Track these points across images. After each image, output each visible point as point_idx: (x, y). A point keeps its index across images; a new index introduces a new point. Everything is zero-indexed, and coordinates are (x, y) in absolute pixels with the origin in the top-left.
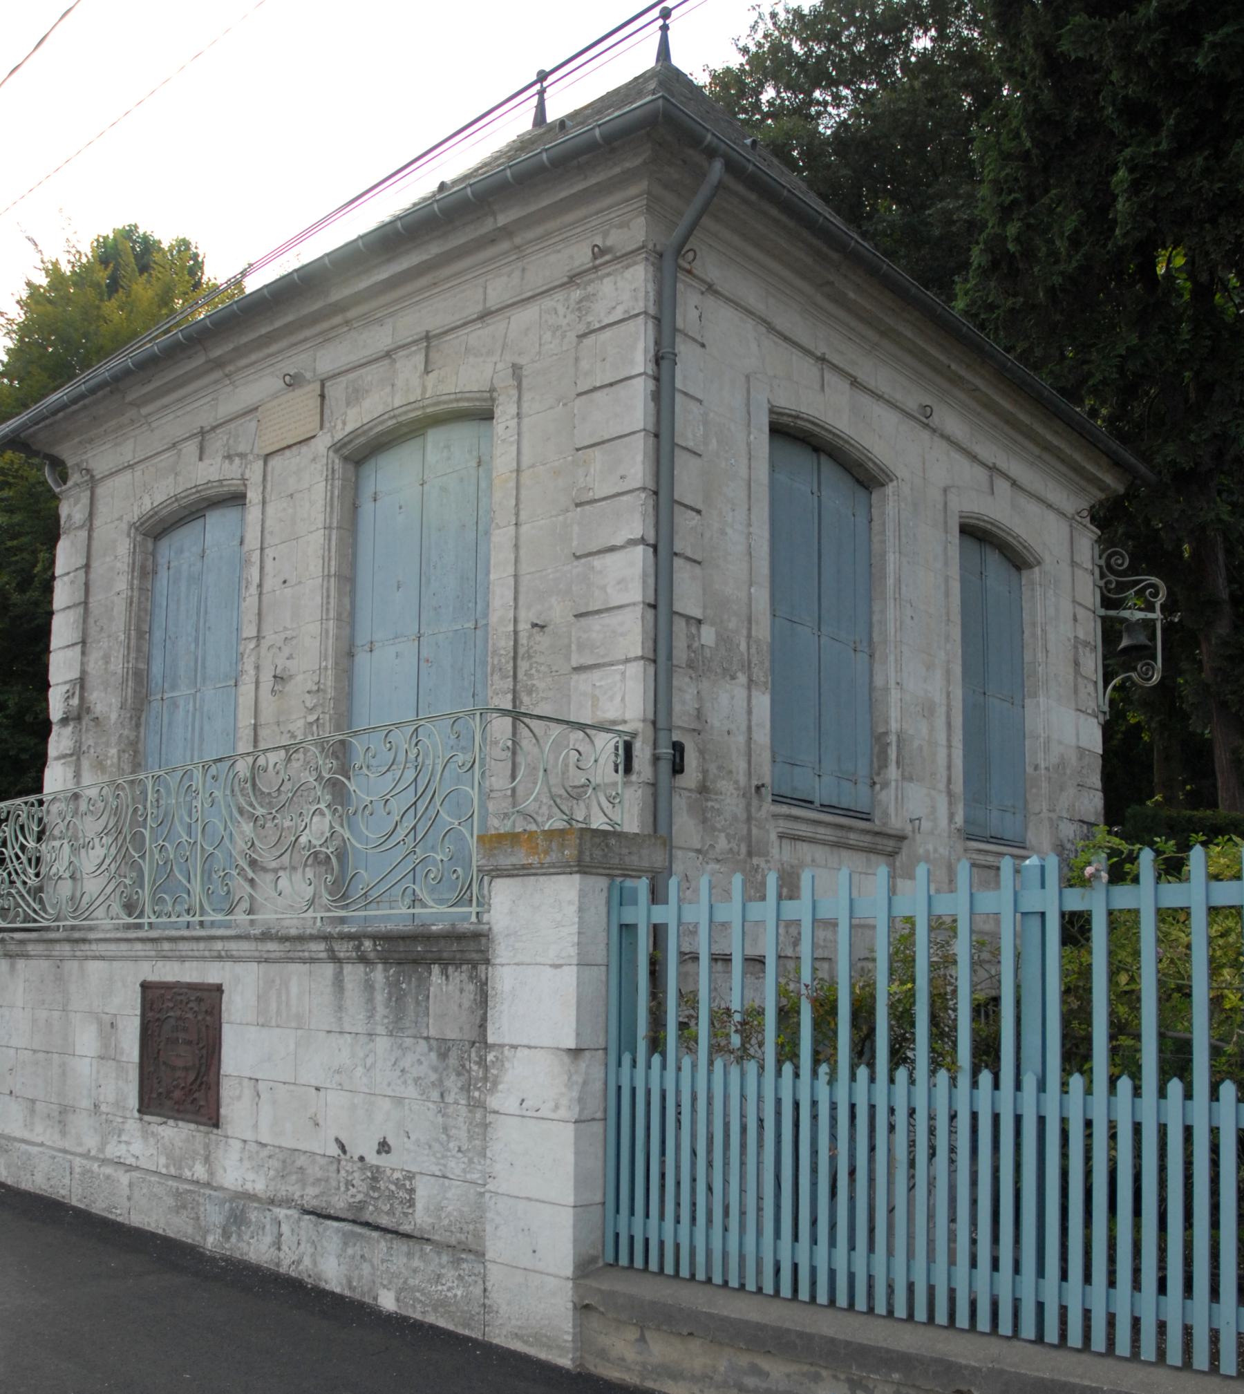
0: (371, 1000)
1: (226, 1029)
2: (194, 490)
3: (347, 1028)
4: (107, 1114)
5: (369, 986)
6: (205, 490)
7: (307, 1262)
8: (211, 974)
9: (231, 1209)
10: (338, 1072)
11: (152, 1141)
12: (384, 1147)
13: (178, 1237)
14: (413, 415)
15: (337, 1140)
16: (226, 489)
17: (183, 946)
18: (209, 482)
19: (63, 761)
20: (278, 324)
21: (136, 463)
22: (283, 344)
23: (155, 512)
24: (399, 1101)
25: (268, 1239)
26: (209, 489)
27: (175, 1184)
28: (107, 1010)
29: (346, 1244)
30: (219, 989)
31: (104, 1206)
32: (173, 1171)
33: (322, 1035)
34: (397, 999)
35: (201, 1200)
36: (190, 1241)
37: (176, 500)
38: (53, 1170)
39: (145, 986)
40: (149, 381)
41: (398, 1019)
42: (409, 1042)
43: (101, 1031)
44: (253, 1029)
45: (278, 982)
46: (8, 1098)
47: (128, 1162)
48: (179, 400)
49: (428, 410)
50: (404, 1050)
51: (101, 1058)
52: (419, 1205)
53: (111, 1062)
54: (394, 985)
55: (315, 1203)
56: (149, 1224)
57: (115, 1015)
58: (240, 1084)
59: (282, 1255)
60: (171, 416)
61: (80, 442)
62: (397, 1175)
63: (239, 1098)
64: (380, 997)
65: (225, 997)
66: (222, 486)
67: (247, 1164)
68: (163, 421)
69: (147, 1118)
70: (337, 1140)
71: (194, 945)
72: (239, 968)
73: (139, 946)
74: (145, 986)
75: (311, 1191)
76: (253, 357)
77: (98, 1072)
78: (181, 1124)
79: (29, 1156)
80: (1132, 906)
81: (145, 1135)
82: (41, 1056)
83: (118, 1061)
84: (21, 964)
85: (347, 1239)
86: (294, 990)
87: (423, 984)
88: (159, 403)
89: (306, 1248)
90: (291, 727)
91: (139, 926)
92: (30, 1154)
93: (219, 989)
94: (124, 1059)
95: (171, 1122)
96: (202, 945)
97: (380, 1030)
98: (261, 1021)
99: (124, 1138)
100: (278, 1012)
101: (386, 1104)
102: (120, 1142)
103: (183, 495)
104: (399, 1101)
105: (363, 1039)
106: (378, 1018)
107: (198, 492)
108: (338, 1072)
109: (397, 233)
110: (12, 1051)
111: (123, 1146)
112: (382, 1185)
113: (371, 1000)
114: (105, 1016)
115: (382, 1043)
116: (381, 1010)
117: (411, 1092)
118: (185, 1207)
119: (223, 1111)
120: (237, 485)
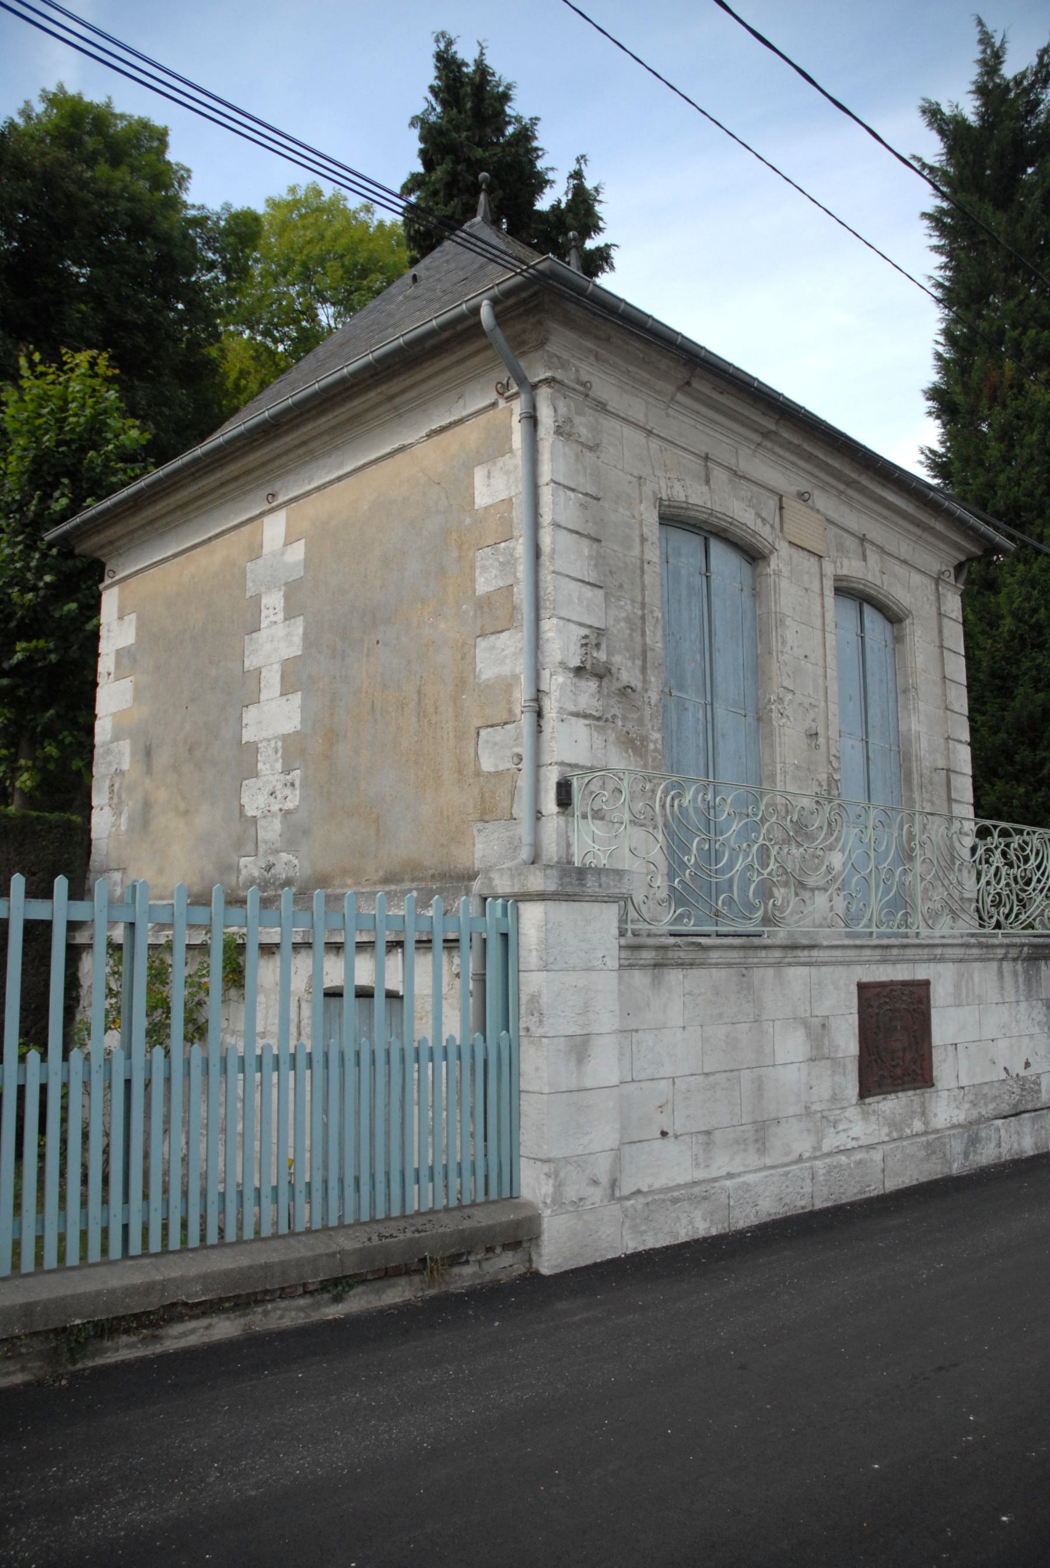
0: (1016, 982)
1: (933, 1011)
2: (730, 520)
3: (1007, 1000)
4: (821, 1112)
5: (1015, 974)
6: (736, 526)
7: (1015, 1146)
8: (921, 973)
9: (970, 1136)
10: (1003, 1027)
11: (873, 1118)
12: (1027, 1064)
13: (930, 1178)
14: (872, 592)
15: (1005, 1069)
16: (753, 540)
17: (909, 952)
18: (745, 524)
19: (587, 722)
20: (830, 461)
21: (658, 436)
22: (808, 467)
23: (687, 506)
24: (1031, 1036)
25: (993, 1145)
26: (741, 529)
27: (924, 1139)
28: (816, 1013)
29: (1034, 1124)
30: (926, 983)
31: (855, 1191)
32: (895, 1135)
33: (994, 1006)
34: (1028, 980)
35: (947, 1140)
36: (939, 1176)
37: (711, 514)
38: (787, 1186)
39: (862, 987)
40: (721, 393)
41: (1030, 991)
42: (1034, 1002)
43: (808, 1035)
44: (951, 1009)
45: (966, 975)
46: (659, 1144)
47: (849, 1147)
48: (712, 421)
49: (867, 589)
50: (1032, 1007)
51: (812, 1060)
52: (1043, 1091)
53: (824, 1061)
54: (1026, 972)
55: (995, 1113)
56: (903, 1182)
57: (828, 1017)
58: (946, 1050)
59: (1001, 1150)
60: (692, 422)
61: (591, 351)
62: (1034, 1078)
63: (945, 1060)
64: (1021, 980)
65: (932, 986)
66: (753, 536)
67: (953, 1105)
68: (681, 417)
69: (868, 1100)
70: (1005, 1069)
71: (920, 951)
72: (940, 967)
73: (867, 952)
74: (862, 987)
75: (991, 1106)
76: (787, 455)
77: (809, 1074)
78: (900, 1094)
79: (747, 1187)
80: (45, 917)
81: (865, 1116)
82: (721, 1078)
83: (833, 1059)
84: (673, 976)
85: (1034, 1121)
86: (976, 978)
87: (1039, 969)
88: (697, 406)
89: (1015, 1137)
90: (818, 777)
91: (906, 936)
92: (748, 1184)
93: (926, 983)
94: (840, 1055)
95: (893, 1096)
96: (926, 951)
97: (1022, 998)
98: (957, 1002)
99: (841, 1127)
100: (967, 997)
101: (1026, 1040)
102: (838, 1133)
103: (719, 515)
104: (1031, 1036)
105: (1014, 1005)
106: (1021, 990)
107: (731, 524)
108: (1003, 1027)
109: (725, 372)
110: (663, 1084)
111: (843, 1135)
112: (1027, 1086)
113: (1016, 982)
114: (814, 1020)
115: (1023, 1005)
116: (1022, 987)
117: (1036, 1030)
118: (934, 1153)
119: (935, 1073)
120: (765, 546)
